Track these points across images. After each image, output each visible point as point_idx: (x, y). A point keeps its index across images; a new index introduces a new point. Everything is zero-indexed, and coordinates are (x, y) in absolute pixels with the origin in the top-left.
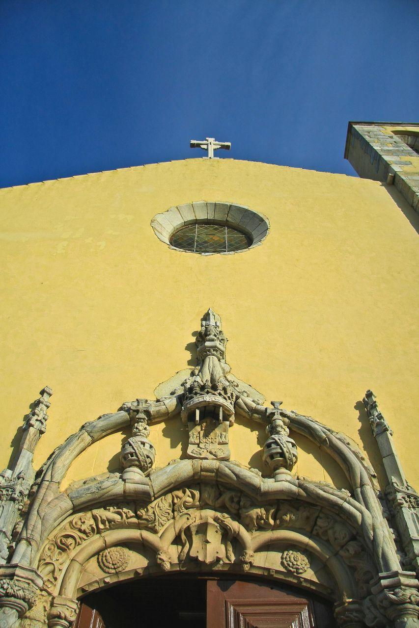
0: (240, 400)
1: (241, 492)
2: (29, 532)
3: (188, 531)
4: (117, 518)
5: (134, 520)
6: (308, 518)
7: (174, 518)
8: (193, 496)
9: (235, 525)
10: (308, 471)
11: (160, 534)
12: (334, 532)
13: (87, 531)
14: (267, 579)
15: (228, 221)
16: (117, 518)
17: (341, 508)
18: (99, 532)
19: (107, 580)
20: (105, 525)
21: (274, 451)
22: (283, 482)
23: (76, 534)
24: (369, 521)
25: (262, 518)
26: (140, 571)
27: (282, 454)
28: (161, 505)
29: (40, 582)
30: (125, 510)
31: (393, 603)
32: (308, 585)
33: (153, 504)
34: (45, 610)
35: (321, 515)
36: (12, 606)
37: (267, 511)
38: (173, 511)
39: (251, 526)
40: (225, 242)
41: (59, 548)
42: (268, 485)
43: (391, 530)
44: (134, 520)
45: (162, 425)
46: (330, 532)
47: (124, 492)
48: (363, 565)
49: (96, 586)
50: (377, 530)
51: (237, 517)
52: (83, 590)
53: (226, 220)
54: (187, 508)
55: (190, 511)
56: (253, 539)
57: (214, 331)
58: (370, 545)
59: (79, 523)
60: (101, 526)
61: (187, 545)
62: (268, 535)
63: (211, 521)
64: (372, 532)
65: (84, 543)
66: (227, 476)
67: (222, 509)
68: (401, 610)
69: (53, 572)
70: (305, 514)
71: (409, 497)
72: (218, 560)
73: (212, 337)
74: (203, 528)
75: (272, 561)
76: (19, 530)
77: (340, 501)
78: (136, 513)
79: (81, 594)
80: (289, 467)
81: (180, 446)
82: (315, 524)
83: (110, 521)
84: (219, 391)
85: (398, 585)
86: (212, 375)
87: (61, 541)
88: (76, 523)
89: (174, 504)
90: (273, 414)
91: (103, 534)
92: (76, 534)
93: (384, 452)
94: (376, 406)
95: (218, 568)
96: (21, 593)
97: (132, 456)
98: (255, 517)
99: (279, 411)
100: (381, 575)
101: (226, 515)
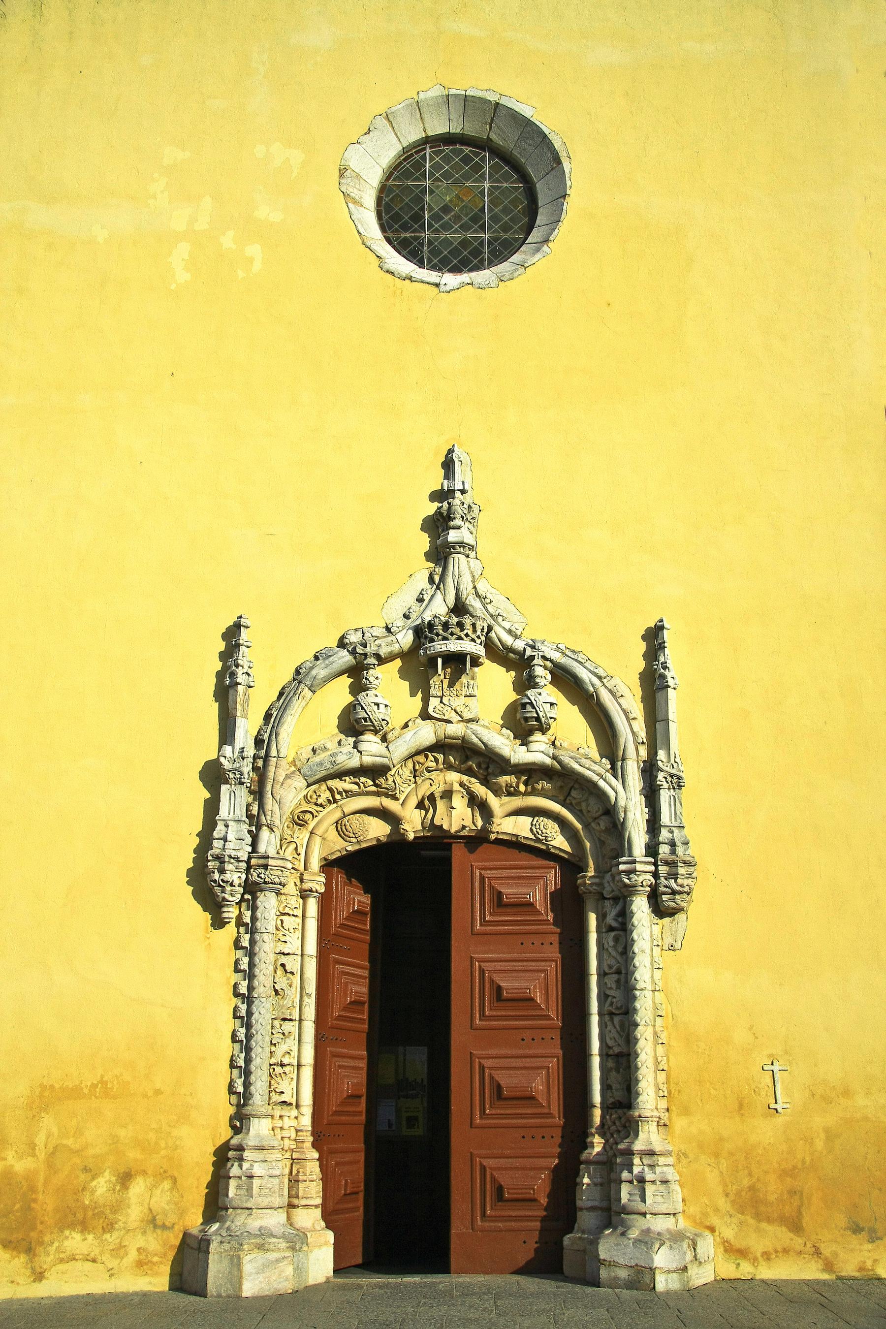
0: (493, 635)
1: (490, 758)
2: (268, 818)
3: (432, 798)
4: (355, 788)
5: (374, 789)
6: (561, 787)
7: (415, 782)
8: (437, 761)
9: (480, 790)
10: (569, 734)
11: (401, 801)
12: (588, 805)
13: (324, 804)
14: (514, 844)
15: (491, 140)
16: (355, 788)
17: (595, 785)
18: (335, 801)
19: (349, 848)
20: (342, 796)
21: (529, 715)
22: (538, 751)
23: (313, 808)
24: (622, 803)
25: (512, 786)
26: (382, 838)
27: (538, 719)
28: (401, 772)
29: (289, 866)
30: (363, 779)
31: (626, 886)
32: (557, 852)
33: (392, 772)
34: (296, 885)
35: (576, 786)
36: (271, 890)
37: (518, 778)
38: (415, 777)
39: (500, 792)
40: (483, 208)
41: (297, 824)
42: (518, 754)
43: (647, 810)
44: (374, 789)
45: (398, 663)
46: (584, 805)
47: (361, 765)
48: (611, 843)
49: (338, 854)
50: (628, 813)
51: (485, 782)
52: (325, 859)
53: (488, 137)
54: (429, 771)
55: (434, 775)
56: (501, 805)
57: (460, 512)
58: (620, 827)
59: (315, 797)
60: (338, 797)
61: (431, 810)
62: (518, 802)
63: (456, 787)
64: (623, 815)
65: (321, 815)
66: (473, 744)
67: (469, 772)
68: (632, 891)
69: (296, 849)
70: (559, 784)
71: (672, 776)
72: (464, 827)
73: (458, 522)
74: (448, 794)
75: (521, 827)
76: (255, 812)
77: (595, 778)
78: (374, 781)
79: (324, 863)
80: (544, 729)
81: (420, 695)
82: (569, 793)
83: (346, 792)
84: (465, 631)
85: (634, 871)
86: (457, 590)
87: (298, 817)
88: (311, 797)
89: (415, 771)
90: (532, 658)
91: (340, 803)
92: (313, 808)
93: (660, 716)
94: (664, 647)
95: (465, 833)
96: (277, 880)
97: (366, 721)
98: (504, 785)
99: (541, 654)
100: (620, 860)
101: (473, 780)
